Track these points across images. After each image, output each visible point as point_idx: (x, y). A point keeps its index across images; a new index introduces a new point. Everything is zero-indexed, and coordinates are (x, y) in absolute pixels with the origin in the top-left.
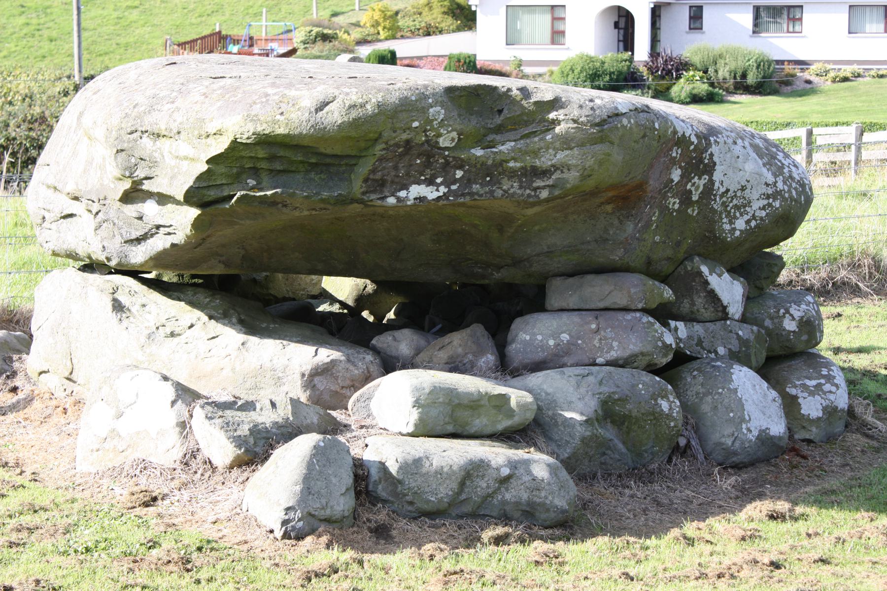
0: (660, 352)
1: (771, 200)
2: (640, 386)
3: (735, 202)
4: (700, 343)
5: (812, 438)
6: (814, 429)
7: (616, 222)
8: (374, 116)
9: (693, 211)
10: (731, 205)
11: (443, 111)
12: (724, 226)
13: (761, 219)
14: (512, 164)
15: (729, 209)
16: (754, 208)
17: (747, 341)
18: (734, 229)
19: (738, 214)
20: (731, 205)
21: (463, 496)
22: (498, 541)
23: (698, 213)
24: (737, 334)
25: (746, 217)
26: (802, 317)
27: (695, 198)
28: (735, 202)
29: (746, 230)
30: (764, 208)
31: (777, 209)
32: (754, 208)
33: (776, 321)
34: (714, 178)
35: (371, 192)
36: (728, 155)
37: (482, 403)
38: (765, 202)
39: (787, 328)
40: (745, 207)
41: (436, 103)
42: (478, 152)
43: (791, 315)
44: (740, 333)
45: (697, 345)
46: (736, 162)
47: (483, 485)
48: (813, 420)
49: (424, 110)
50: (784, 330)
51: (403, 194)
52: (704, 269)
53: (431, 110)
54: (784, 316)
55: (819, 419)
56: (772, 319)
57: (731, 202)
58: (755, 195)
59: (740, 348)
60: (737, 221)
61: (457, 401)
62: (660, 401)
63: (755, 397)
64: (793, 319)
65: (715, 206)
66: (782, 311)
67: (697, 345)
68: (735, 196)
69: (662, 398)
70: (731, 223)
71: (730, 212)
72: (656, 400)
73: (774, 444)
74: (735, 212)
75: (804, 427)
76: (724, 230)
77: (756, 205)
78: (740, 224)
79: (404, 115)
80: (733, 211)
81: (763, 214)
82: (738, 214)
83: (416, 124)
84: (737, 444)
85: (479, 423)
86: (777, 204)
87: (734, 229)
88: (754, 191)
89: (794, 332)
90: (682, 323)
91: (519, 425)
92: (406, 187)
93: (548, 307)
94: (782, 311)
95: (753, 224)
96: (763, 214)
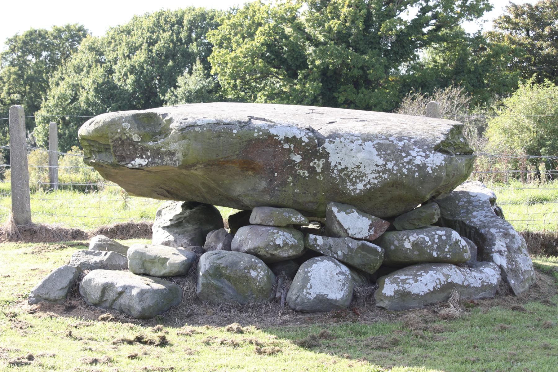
0: (271, 248)
1: (381, 174)
2: (242, 262)
3: (354, 174)
4: (330, 248)
5: (384, 306)
6: (387, 302)
7: (258, 181)
8: (102, 126)
9: (320, 177)
10: (352, 176)
11: (130, 125)
12: (348, 187)
13: (374, 184)
14: (163, 149)
15: (351, 178)
16: (369, 178)
17: (353, 249)
18: (356, 189)
19: (358, 181)
20: (352, 176)
21: (105, 299)
22: (104, 319)
23: (323, 179)
24: (348, 245)
25: (364, 183)
26: (414, 241)
27: (319, 170)
28: (354, 174)
29: (364, 189)
30: (376, 178)
31: (385, 179)
32: (369, 178)
33: (401, 242)
34: (329, 160)
35: (121, 161)
36: (344, 149)
37: (155, 261)
38: (377, 175)
39: (406, 247)
40: (362, 177)
41: (125, 121)
42: (151, 143)
43: (409, 240)
44: (350, 245)
45: (328, 249)
46: (350, 152)
47: (111, 296)
48: (388, 297)
49: (120, 124)
50: (404, 247)
51: (133, 162)
52: (335, 209)
53: (123, 124)
54: (405, 240)
55: (391, 296)
56: (399, 241)
57: (352, 174)
58: (368, 171)
59: (348, 253)
60: (358, 185)
61: (144, 259)
62: (251, 271)
63: (323, 277)
64: (410, 242)
65: (333, 175)
66: (405, 237)
67: (328, 249)
68: (354, 171)
69: (253, 270)
70: (353, 185)
71: (352, 180)
72: (249, 270)
73: (331, 304)
74: (356, 180)
75: (382, 300)
76: (349, 189)
77: (370, 177)
78: (360, 186)
79: (113, 127)
80: (354, 179)
81: (376, 181)
82: (358, 181)
83: (119, 131)
84: (299, 299)
85: (154, 271)
86: (386, 176)
87: (356, 189)
88: (367, 168)
89: (409, 249)
90: (321, 237)
91: (169, 273)
92: (133, 159)
93: (251, 222)
94: (405, 237)
95: (369, 186)
96: (376, 181)
